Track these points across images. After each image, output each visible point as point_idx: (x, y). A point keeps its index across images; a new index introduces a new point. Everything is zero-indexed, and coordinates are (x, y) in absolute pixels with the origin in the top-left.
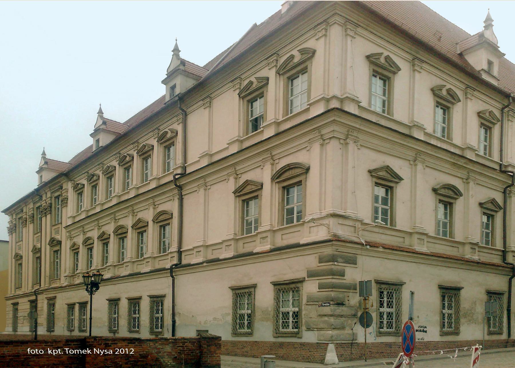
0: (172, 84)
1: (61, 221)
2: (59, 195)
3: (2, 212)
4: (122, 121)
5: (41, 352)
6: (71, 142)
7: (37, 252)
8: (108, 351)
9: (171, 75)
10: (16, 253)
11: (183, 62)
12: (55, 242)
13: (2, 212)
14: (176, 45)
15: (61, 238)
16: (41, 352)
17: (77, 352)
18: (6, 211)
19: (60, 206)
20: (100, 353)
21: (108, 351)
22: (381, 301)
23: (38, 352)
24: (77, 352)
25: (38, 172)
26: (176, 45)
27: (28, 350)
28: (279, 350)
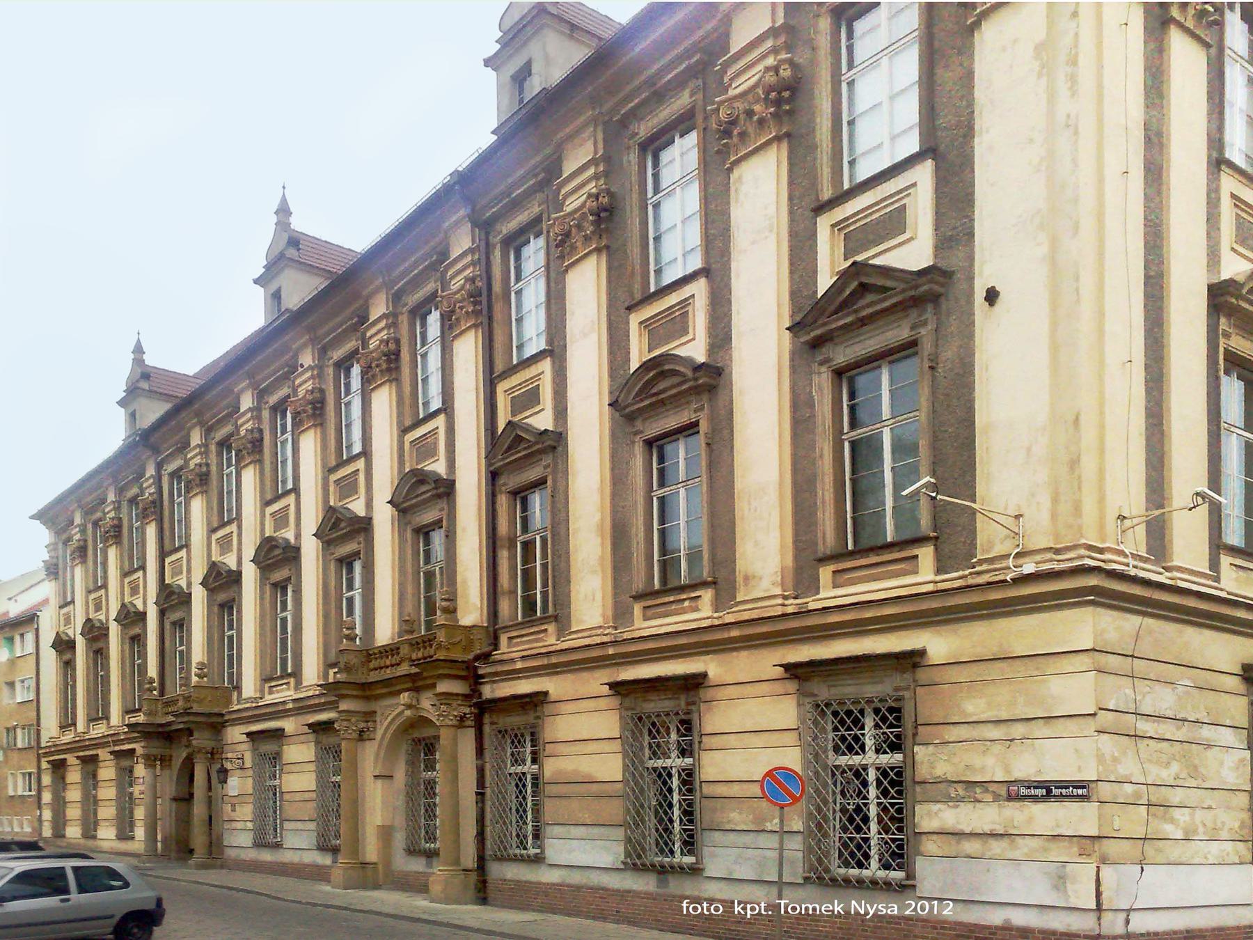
0: (273, 287)
1: (296, 478)
2: (181, 468)
3: (33, 517)
4: (487, 140)
5: (717, 909)
6: (213, 317)
7: (133, 623)
8: (887, 908)
9: (275, 265)
10: (89, 620)
11: (295, 241)
12: (277, 552)
13: (33, 517)
14: (284, 200)
15: (240, 563)
16: (717, 909)
17: (807, 909)
18: (41, 516)
19: (288, 436)
20: (867, 913)
21: (887, 908)
22: (690, 791)
23: (708, 910)
24: (807, 909)
25: (122, 403)
26: (284, 200)
27: (685, 905)
28: (746, 903)
